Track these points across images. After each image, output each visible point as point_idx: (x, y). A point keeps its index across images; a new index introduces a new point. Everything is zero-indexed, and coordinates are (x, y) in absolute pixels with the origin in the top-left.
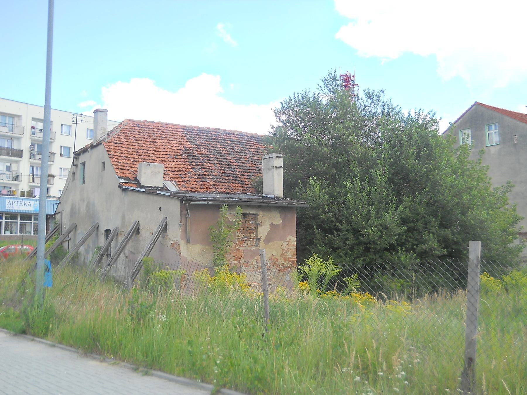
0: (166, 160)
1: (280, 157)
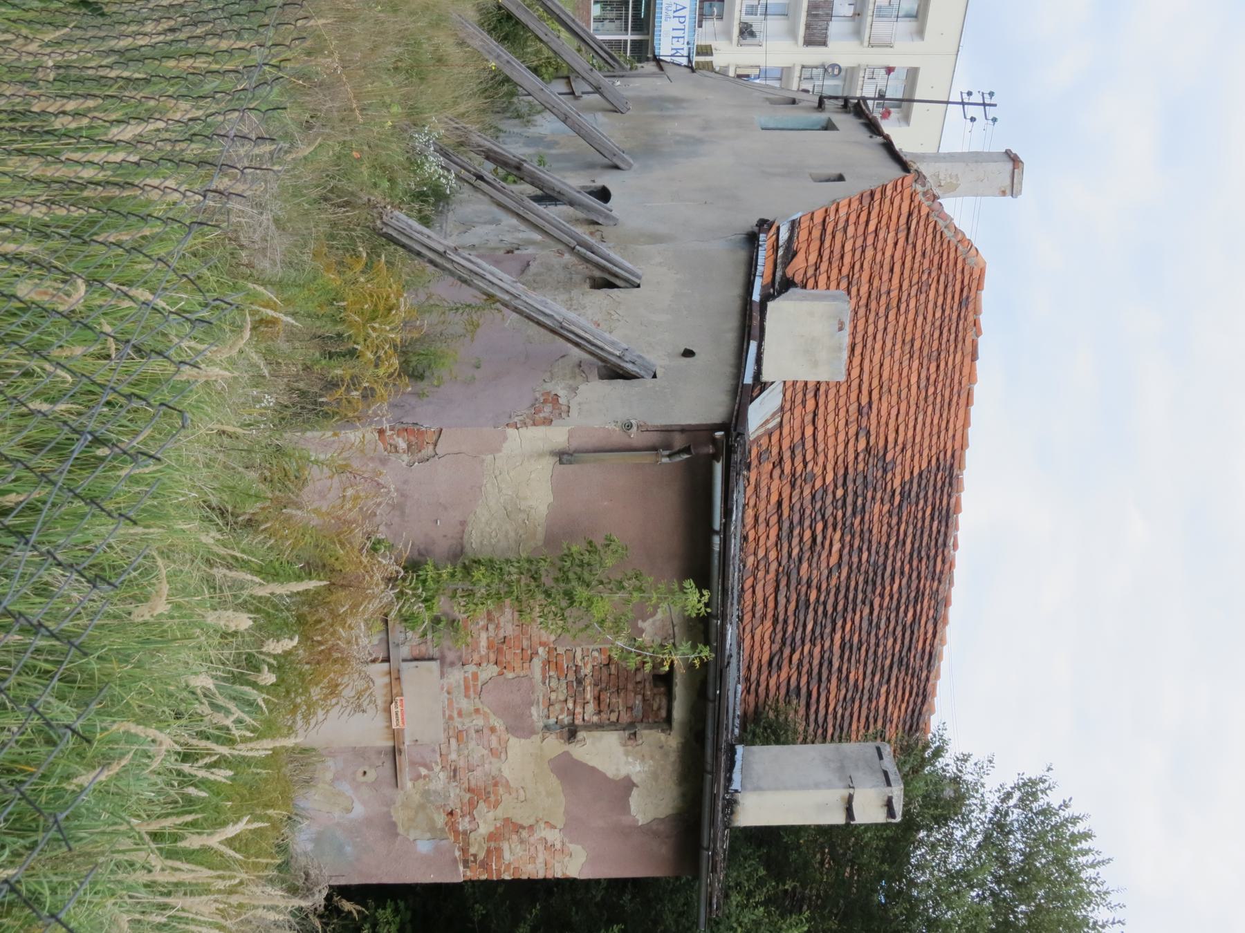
0: (853, 396)
1: (891, 813)
